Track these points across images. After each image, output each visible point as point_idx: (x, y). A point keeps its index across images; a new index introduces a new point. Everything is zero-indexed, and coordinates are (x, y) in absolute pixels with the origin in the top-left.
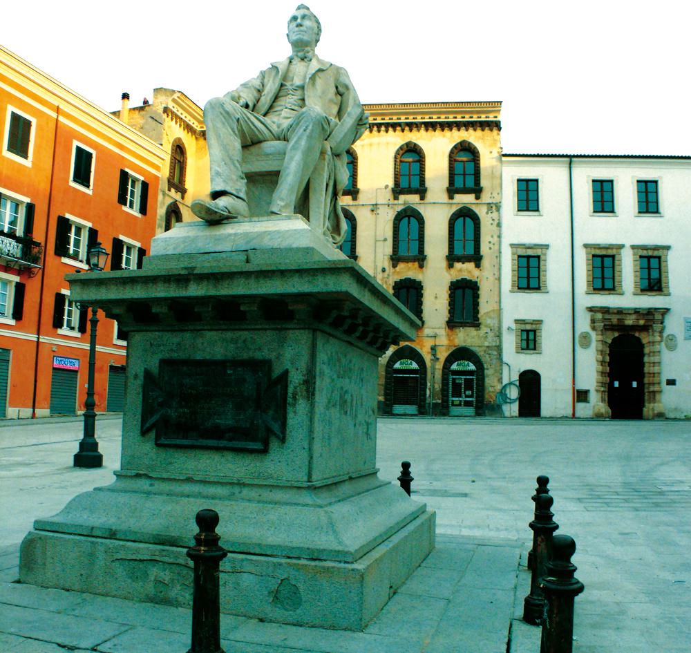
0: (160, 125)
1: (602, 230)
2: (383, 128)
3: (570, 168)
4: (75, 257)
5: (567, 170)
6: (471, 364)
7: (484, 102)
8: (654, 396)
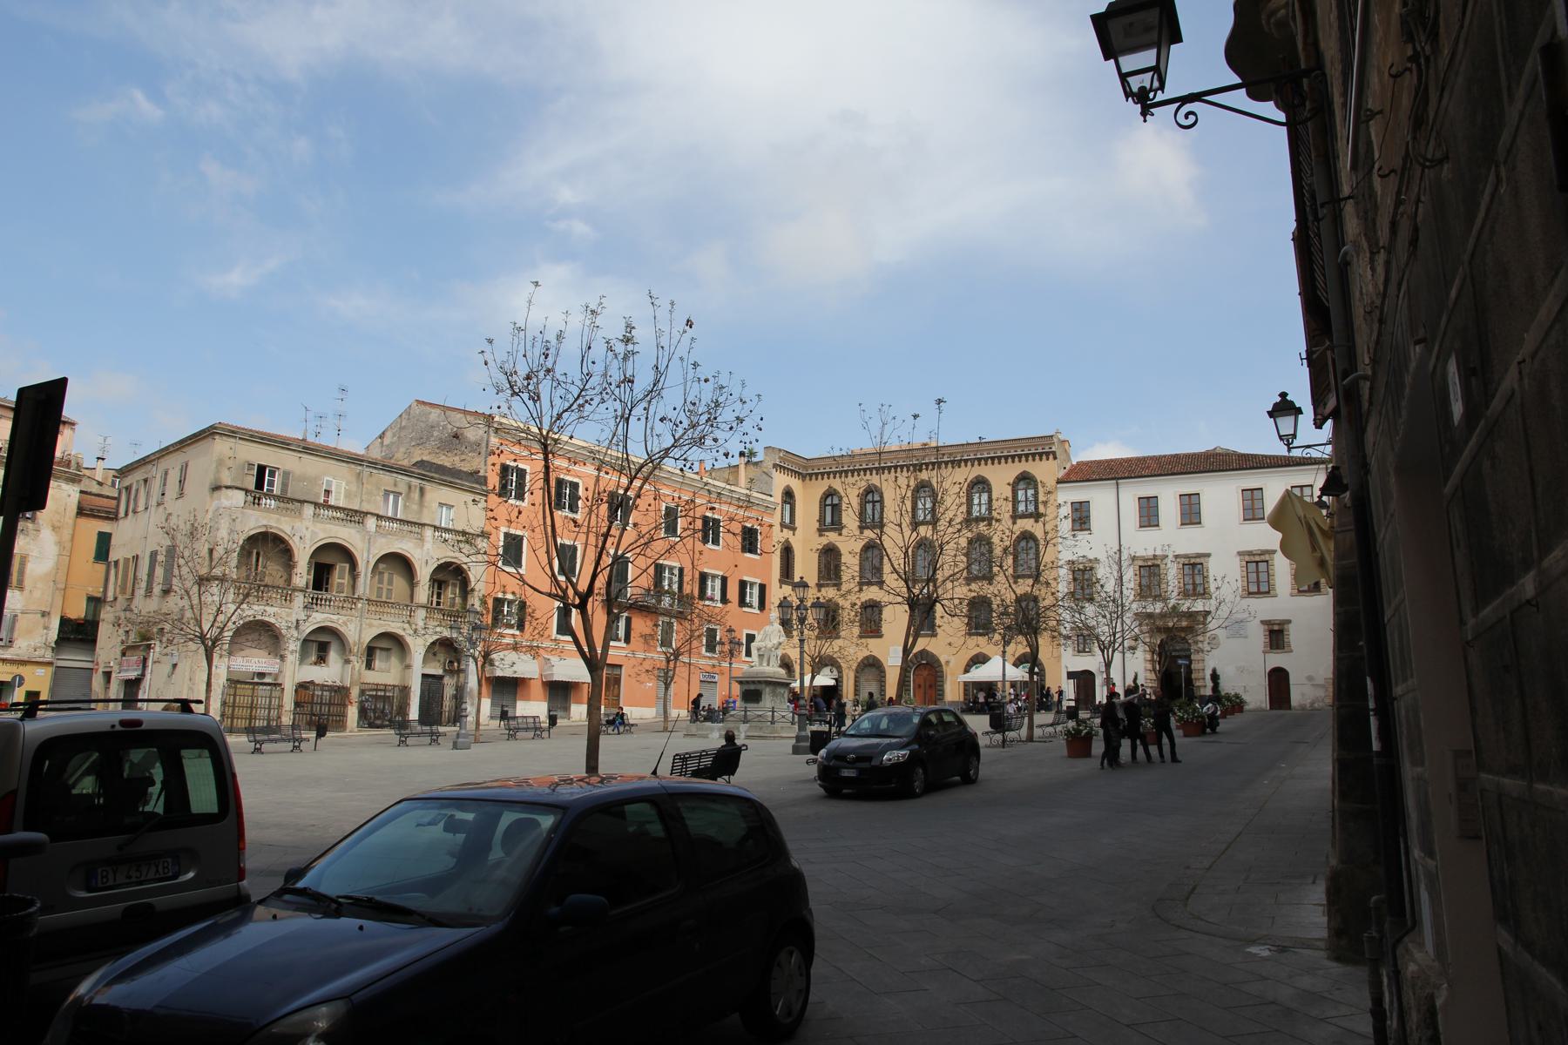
1: (1144, 543)
2: (1037, 457)
3: (1118, 488)
4: (712, 599)
5: (1115, 490)
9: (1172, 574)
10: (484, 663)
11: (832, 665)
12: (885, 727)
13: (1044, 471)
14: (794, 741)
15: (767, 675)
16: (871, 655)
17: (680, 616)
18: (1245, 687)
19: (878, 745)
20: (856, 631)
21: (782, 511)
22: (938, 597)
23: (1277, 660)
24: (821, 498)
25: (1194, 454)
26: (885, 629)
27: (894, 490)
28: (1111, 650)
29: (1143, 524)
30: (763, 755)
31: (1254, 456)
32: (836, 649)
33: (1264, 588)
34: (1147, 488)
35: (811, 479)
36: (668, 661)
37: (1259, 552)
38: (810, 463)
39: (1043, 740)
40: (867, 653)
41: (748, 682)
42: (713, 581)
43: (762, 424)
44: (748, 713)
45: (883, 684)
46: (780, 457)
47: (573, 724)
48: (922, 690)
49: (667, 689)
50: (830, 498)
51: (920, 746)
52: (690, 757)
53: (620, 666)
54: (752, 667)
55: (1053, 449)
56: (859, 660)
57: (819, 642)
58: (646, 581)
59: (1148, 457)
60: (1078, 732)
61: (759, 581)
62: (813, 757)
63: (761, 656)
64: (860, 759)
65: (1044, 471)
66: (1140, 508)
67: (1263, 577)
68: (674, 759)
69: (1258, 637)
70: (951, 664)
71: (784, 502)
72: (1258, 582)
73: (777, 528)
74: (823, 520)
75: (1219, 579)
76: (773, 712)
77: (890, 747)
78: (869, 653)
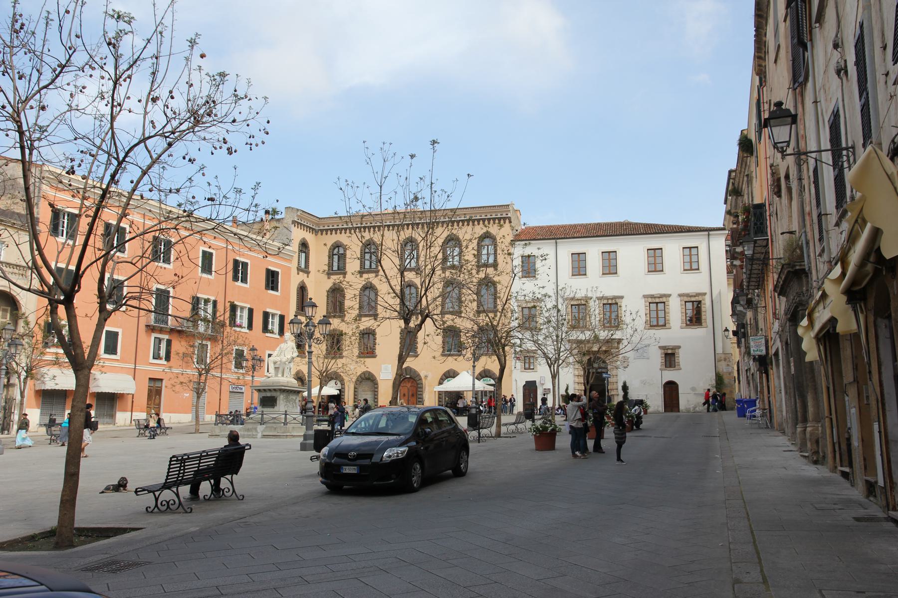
1: (656, 285)
3: (709, 238)
9: (595, 309)
10: (27, 377)
11: (336, 379)
12: (384, 425)
13: (504, 234)
14: (302, 439)
15: (282, 384)
17: (213, 339)
18: (647, 396)
19: (377, 443)
20: (356, 352)
23: (670, 375)
25: (611, 224)
26: (378, 350)
27: (390, 240)
28: (556, 365)
29: (574, 273)
31: (656, 225)
32: (340, 365)
33: (661, 322)
34: (578, 246)
35: (322, 234)
36: (200, 375)
37: (659, 296)
41: (265, 390)
42: (242, 312)
43: (269, 128)
44: (265, 416)
45: (376, 393)
46: (298, 216)
47: (118, 428)
48: (406, 397)
49: (198, 397)
50: (337, 249)
51: (417, 443)
52: (189, 458)
53: (161, 380)
55: (509, 215)
56: (358, 374)
57: (326, 360)
58: (186, 310)
59: (578, 225)
60: (546, 429)
62: (317, 454)
63: (277, 369)
64: (361, 456)
65: (504, 234)
67: (661, 314)
68: (171, 461)
69: (657, 358)
70: (428, 378)
71: (301, 251)
72: (657, 318)
73: (294, 270)
74: (331, 264)
75: (634, 313)
76: (286, 415)
77: (389, 445)
78: (365, 369)
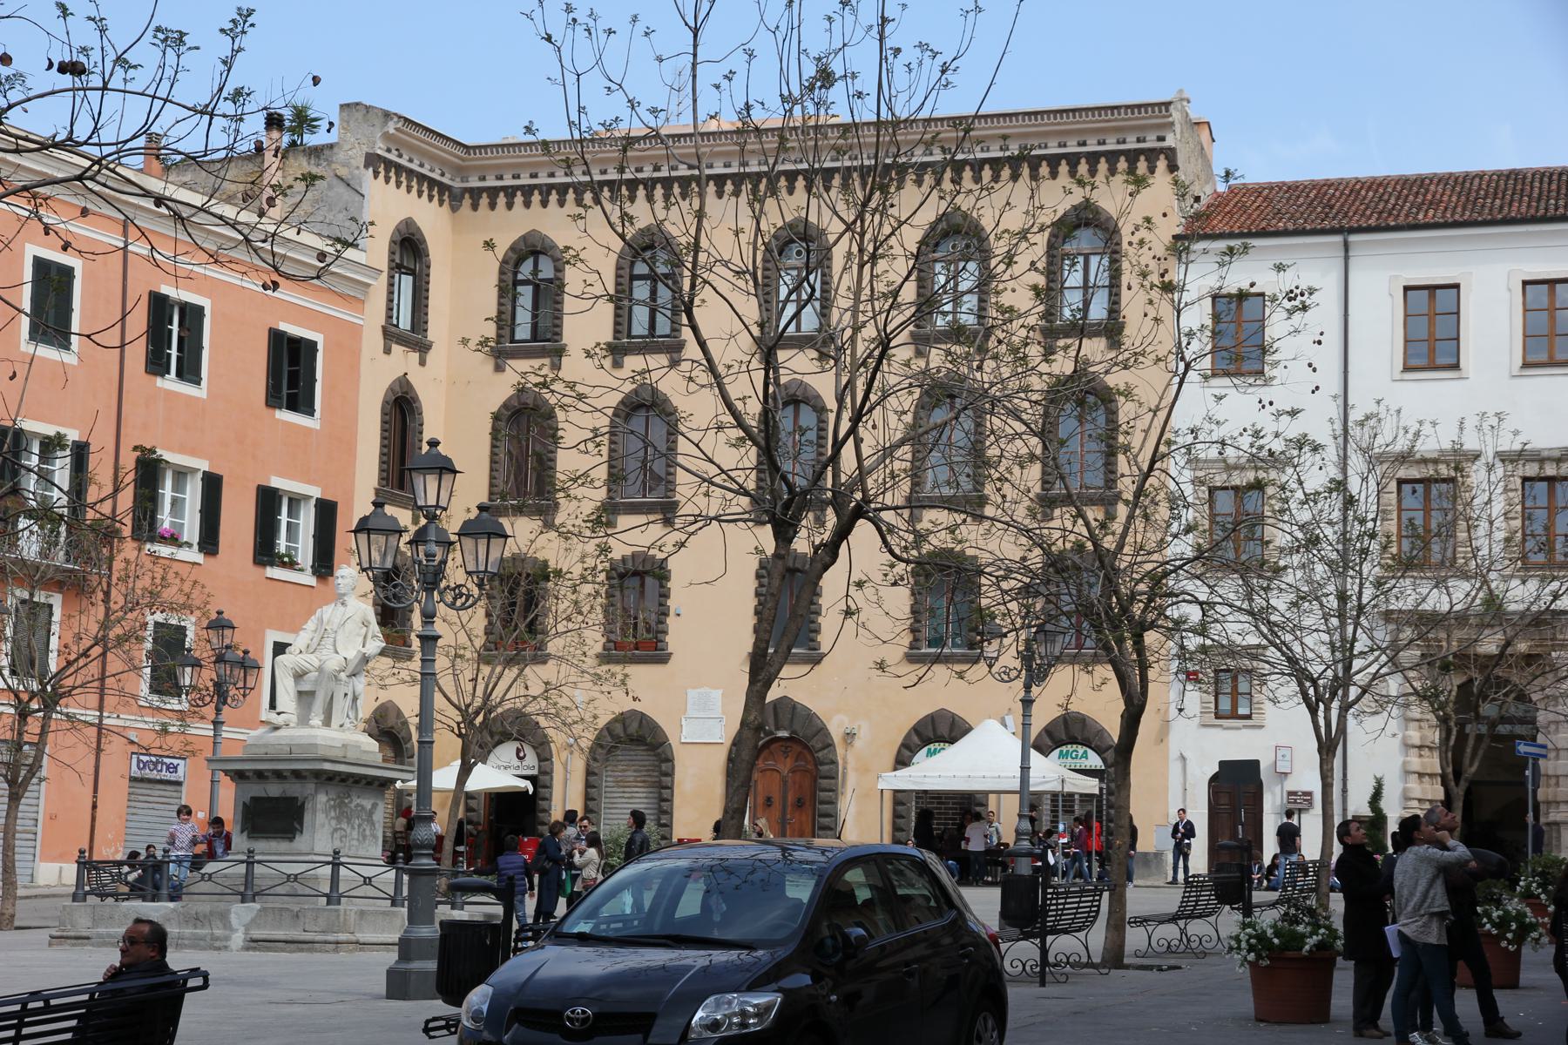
0: (358, 198)
3: (1347, 258)
5: (1342, 261)
6: (1090, 752)
7: (1127, 107)
8: (1559, 832)
14: (392, 957)
15: (321, 753)
16: (633, 712)
17: (73, 586)
19: (668, 974)
20: (595, 640)
21: (391, 293)
22: (866, 500)
24: (504, 262)
26: (677, 635)
28: (1335, 705)
30: (291, 1002)
32: (537, 689)
35: (475, 207)
36: (23, 714)
38: (476, 160)
39: (1162, 961)
40: (627, 705)
41: (260, 775)
42: (179, 486)
45: (666, 793)
46: (387, 137)
51: (817, 978)
54: (277, 728)
55: (1170, 141)
56: (602, 722)
61: (315, 492)
62: (450, 1010)
63: (305, 697)
66: (1406, 316)
70: (858, 743)
71: (397, 268)
73: (373, 338)
74: (508, 317)
76: (336, 866)
